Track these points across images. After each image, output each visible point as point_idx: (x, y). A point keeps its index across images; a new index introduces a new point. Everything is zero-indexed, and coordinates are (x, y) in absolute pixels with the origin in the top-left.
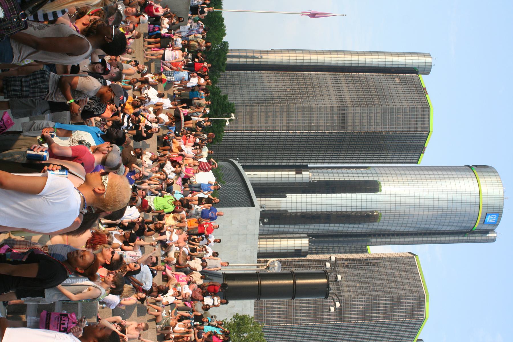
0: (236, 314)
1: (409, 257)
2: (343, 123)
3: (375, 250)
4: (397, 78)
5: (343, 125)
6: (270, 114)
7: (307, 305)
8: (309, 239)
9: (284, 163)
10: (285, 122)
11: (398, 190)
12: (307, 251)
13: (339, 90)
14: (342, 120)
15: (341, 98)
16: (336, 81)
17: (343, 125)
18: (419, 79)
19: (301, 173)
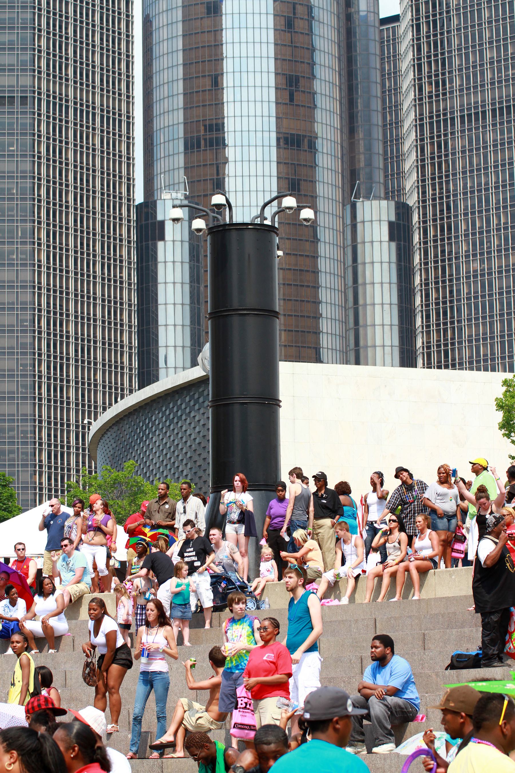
0: (500, 428)
5: (17, 102)
8: (357, 197)
9: (129, 275)
12: (392, 204)
17: (17, 102)
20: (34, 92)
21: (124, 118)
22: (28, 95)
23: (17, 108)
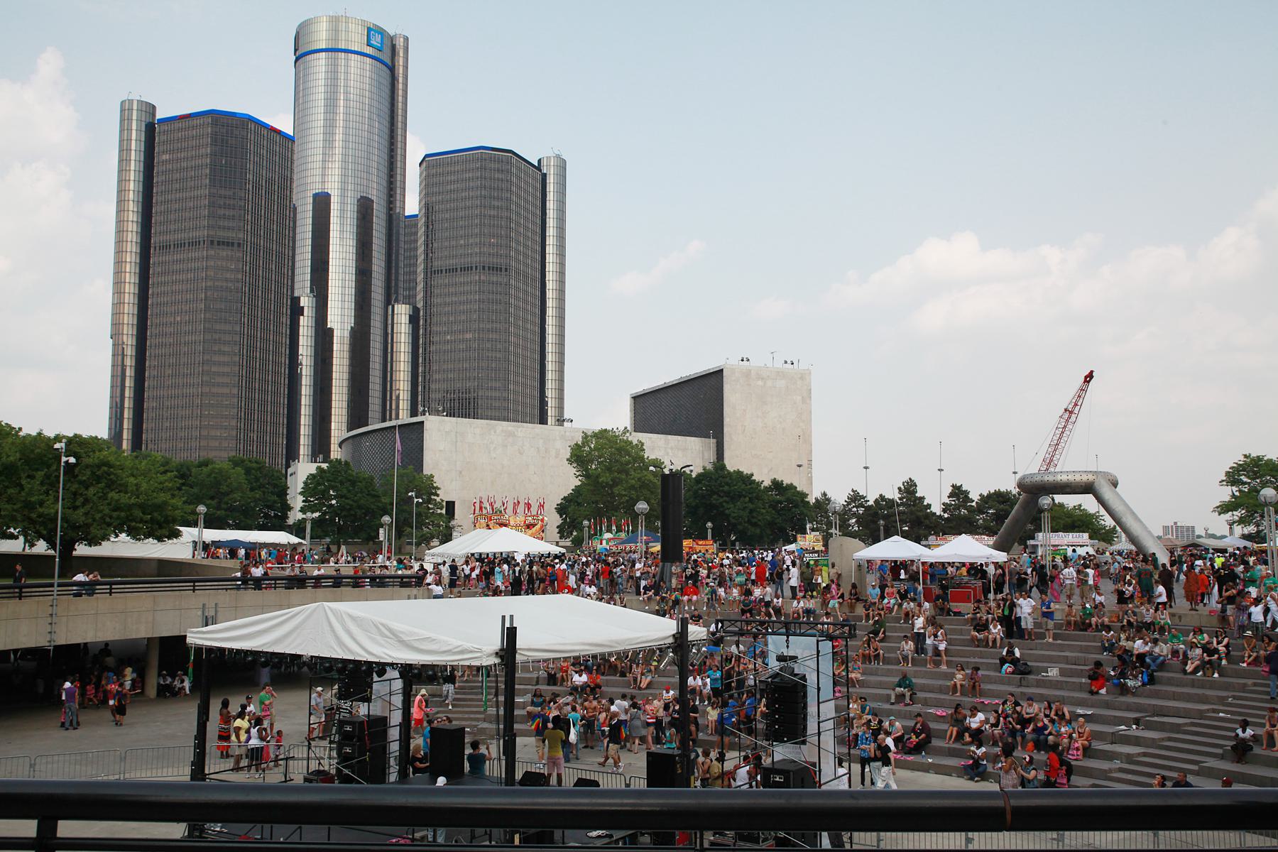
1: (428, 167)
2: (233, 244)
3: (412, 204)
4: (161, 157)
7: (488, 212)
10: (228, 327)
11: (329, 171)
13: (180, 245)
15: (194, 244)
16: (165, 247)
18: (162, 121)
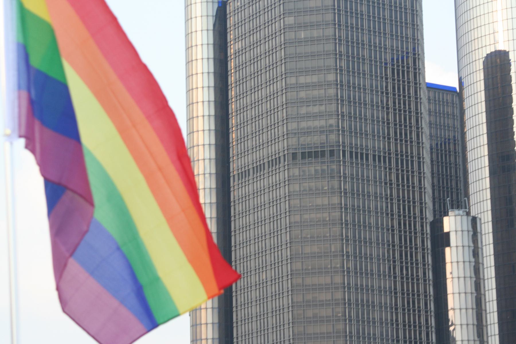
2: (323, 153)
5: (327, 154)
6: (310, 313)
14: (316, 157)
17: (327, 154)
19: (448, 234)
20: (339, 146)
21: (415, 159)
22: (335, 149)
23: (327, 159)
